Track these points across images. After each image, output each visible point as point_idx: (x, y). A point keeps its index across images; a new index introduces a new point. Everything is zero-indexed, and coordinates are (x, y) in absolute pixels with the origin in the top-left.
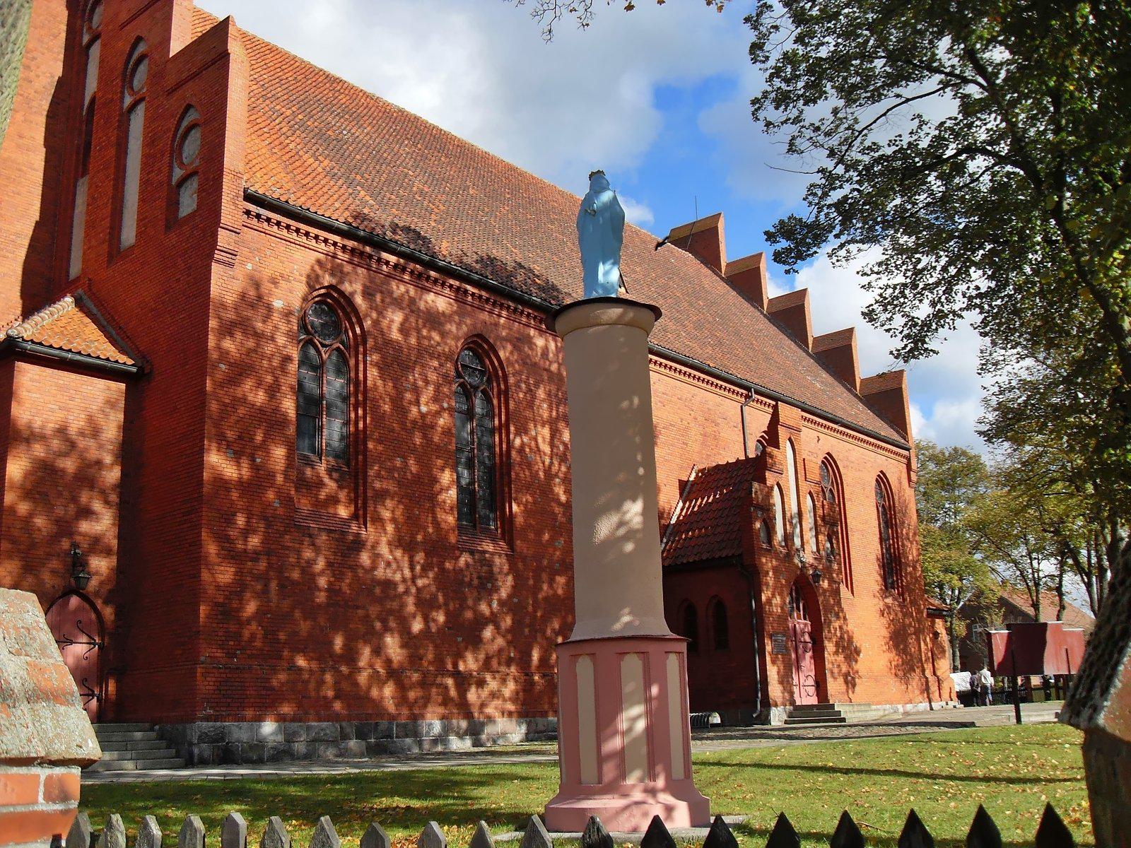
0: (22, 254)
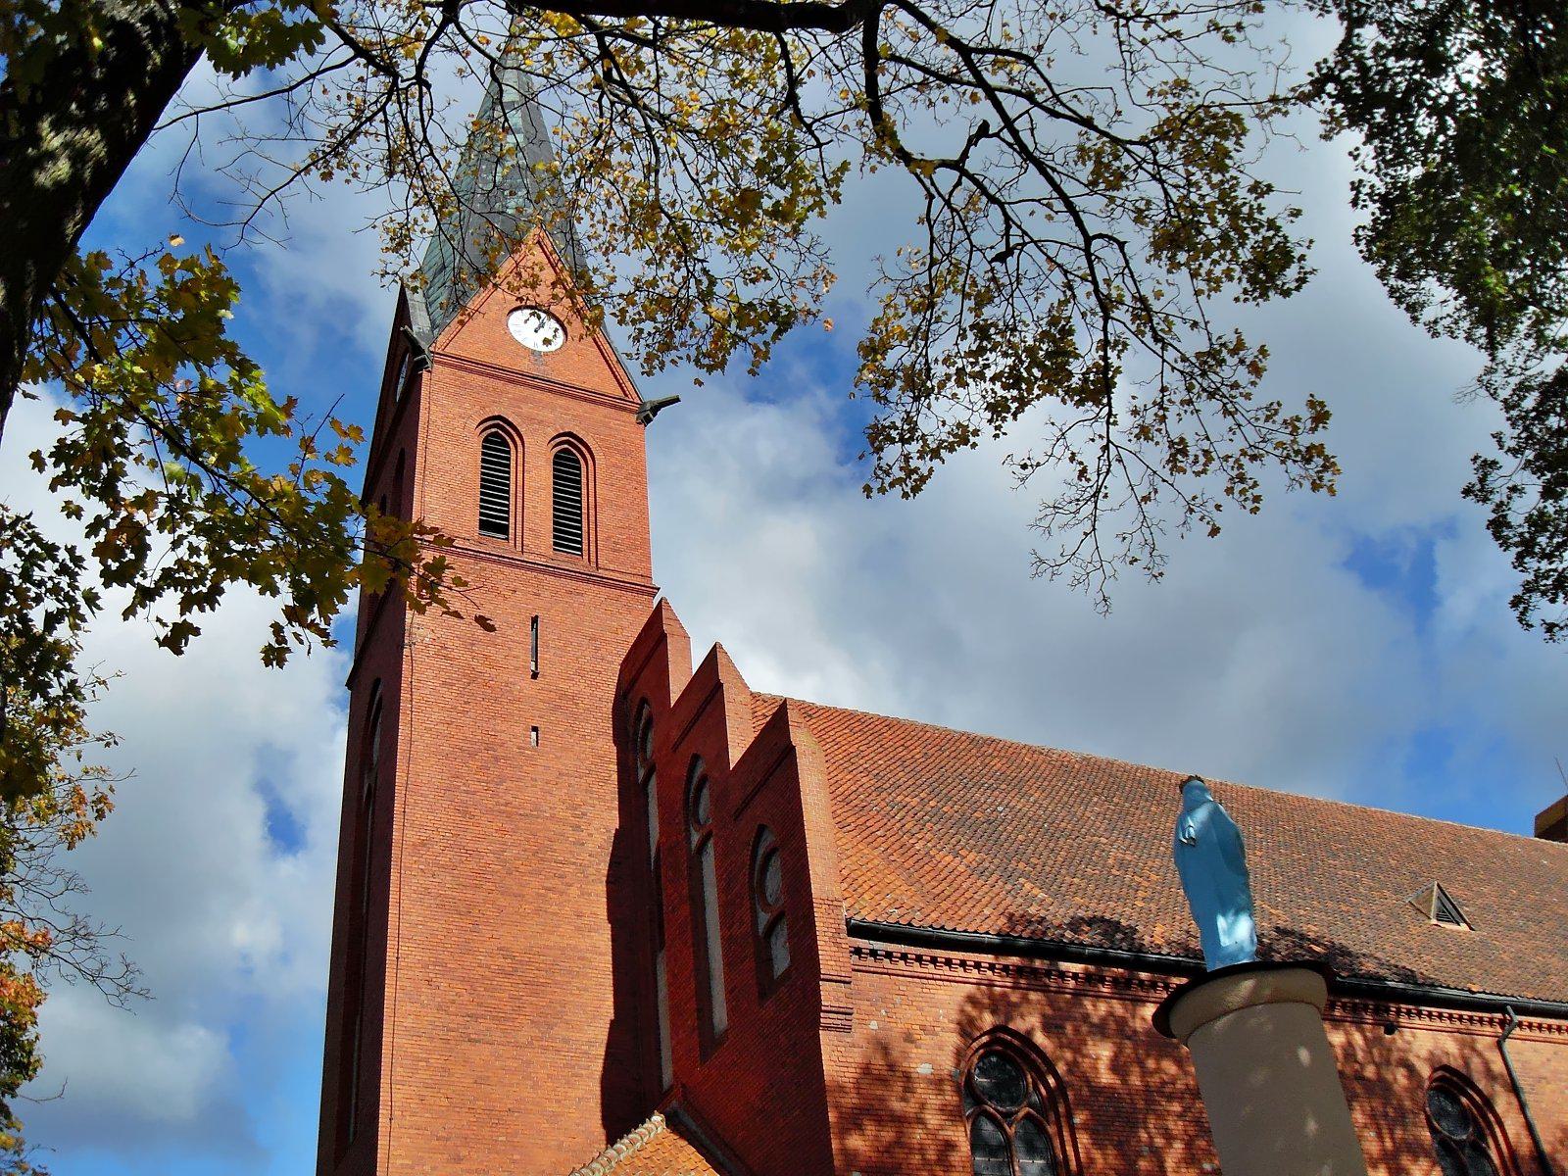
0: (598, 1066)
